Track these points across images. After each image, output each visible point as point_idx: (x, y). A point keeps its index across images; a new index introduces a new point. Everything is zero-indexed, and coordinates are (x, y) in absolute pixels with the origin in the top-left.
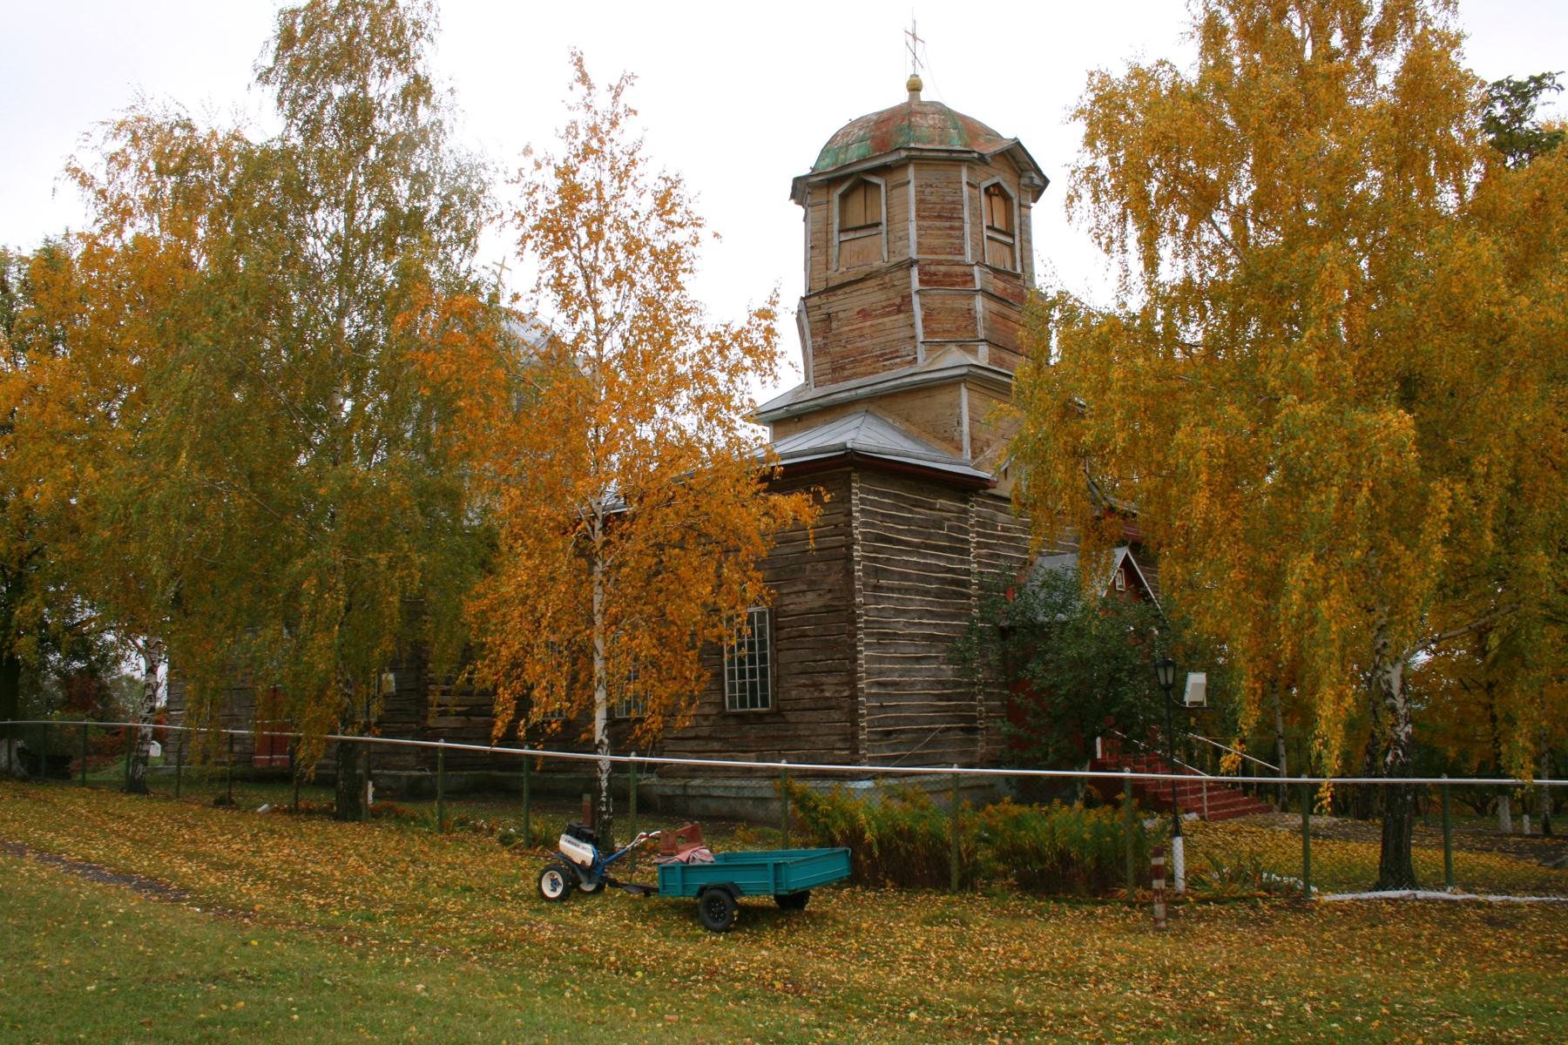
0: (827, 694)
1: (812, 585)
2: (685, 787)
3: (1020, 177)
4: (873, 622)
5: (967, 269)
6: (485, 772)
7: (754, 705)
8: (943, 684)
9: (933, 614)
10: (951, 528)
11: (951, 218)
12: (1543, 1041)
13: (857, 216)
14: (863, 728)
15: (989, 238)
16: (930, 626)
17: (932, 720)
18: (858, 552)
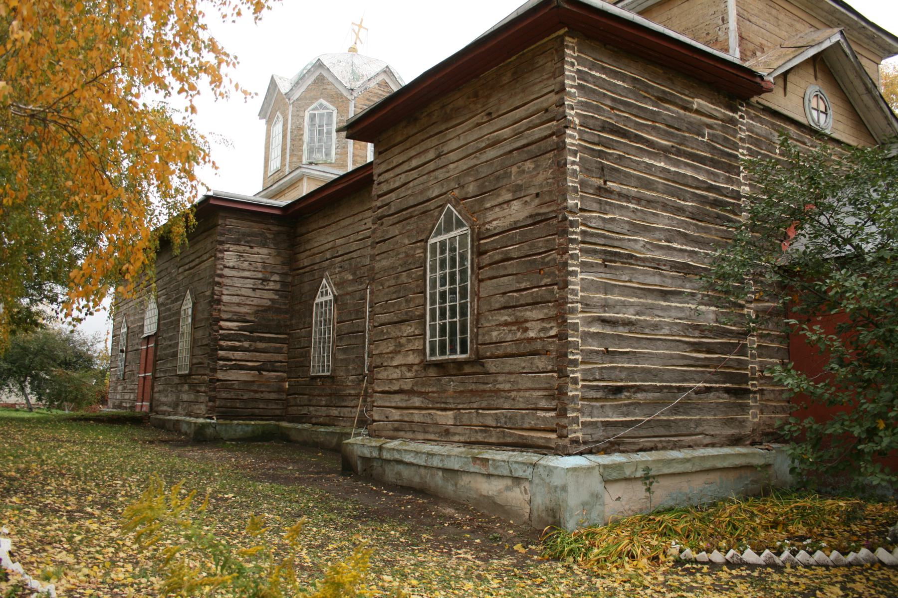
0: (531, 334)
1: (518, 191)
4: (592, 235)
6: (273, 422)
7: (453, 351)
10: (712, 137)
14: (575, 381)
18: (572, 139)
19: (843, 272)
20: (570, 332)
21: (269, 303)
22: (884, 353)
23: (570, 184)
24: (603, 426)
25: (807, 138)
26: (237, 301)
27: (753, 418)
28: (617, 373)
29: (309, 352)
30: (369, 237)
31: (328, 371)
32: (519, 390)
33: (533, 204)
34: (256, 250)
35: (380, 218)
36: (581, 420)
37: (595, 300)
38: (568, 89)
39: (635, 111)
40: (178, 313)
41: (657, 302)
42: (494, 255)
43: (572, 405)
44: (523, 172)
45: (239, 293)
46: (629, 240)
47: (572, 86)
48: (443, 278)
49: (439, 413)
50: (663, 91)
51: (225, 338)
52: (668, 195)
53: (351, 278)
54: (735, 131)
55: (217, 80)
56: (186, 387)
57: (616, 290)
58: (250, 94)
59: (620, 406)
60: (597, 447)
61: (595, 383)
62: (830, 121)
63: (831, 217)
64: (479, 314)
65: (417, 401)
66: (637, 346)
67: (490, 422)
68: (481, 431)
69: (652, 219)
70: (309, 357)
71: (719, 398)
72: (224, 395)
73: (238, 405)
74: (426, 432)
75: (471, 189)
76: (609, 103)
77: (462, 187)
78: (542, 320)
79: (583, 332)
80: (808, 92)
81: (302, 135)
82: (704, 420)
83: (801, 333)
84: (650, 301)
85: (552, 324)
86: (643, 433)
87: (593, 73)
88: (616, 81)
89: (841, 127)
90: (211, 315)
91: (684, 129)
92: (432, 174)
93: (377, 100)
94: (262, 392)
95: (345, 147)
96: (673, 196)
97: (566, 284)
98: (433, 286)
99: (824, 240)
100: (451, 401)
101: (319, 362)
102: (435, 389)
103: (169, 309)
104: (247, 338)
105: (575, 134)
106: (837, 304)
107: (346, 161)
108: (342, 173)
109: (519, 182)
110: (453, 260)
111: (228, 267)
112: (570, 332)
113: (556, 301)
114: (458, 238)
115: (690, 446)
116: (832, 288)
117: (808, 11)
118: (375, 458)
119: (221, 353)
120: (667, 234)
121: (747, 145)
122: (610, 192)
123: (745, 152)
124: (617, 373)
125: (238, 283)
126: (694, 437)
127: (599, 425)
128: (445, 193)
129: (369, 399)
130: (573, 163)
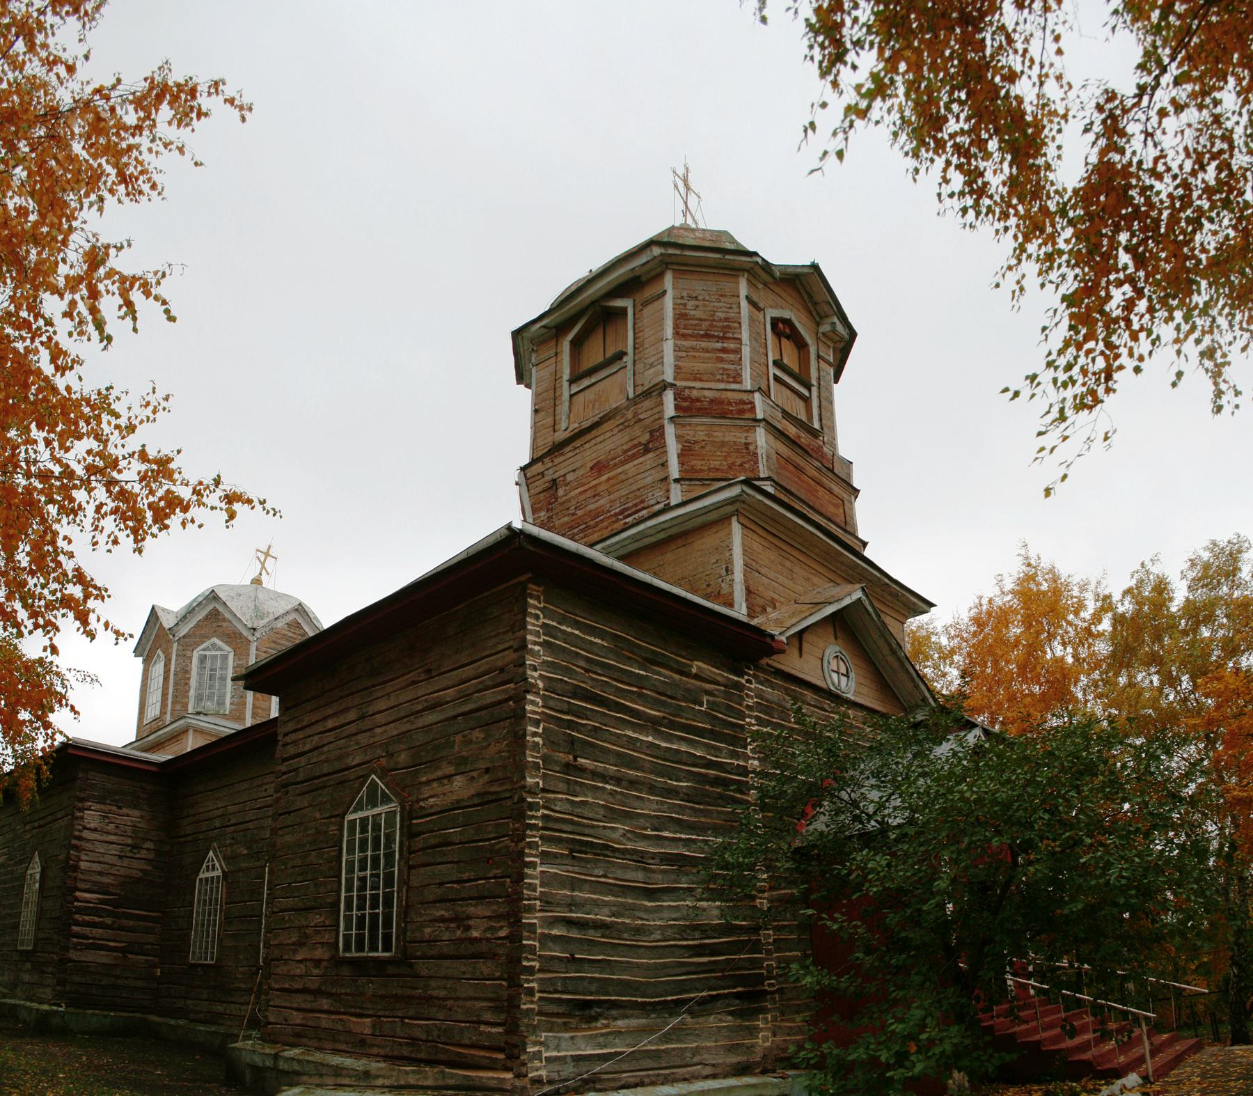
0: (475, 934)
1: (462, 766)
2: (276, 1057)
3: (818, 324)
4: (557, 820)
5: (745, 397)
8: (705, 930)
9: (682, 825)
11: (724, 339)
13: (594, 353)
14: (530, 992)
15: (776, 378)
16: (675, 842)
17: (682, 987)
18: (534, 705)
19: (864, 853)
20: (525, 934)
21: (140, 874)
22: (911, 935)
23: (530, 759)
24: (573, 1061)
25: (827, 704)
26: (99, 869)
27: (764, 1042)
28: (586, 984)
29: (189, 935)
30: (270, 806)
31: (212, 959)
32: (457, 999)
33: (481, 781)
34: (125, 811)
35: (285, 786)
36: (545, 1055)
37: (558, 897)
38: (530, 646)
39: (616, 675)
40: (23, 877)
41: (638, 902)
42: (429, 838)
43: (533, 1038)
44: (471, 742)
45: (101, 859)
46: (605, 827)
47: (535, 643)
48: (363, 862)
49: (354, 1019)
50: (654, 651)
51: (81, 911)
52: (658, 775)
53: (245, 852)
54: (741, 697)
55: (83, 617)
56: (28, 966)
57: (587, 886)
58: (123, 635)
59: (596, 1036)
60: (566, 1086)
61: (556, 996)
62: (853, 684)
63: (852, 791)
64: (408, 906)
65: (325, 1003)
66: (612, 953)
67: (418, 1033)
68: (407, 1044)
69: (636, 804)
70: (189, 940)
71: (721, 1021)
72: (77, 979)
73: (94, 992)
74: (335, 1041)
75: (403, 758)
76: (582, 664)
77: (390, 755)
78: (490, 918)
79: (542, 934)
80: (827, 653)
81: (189, 679)
82: (703, 1048)
83: (820, 923)
84: (630, 901)
85: (502, 924)
86: (625, 1067)
87: (564, 628)
88: (592, 639)
89: (865, 690)
90: (65, 883)
91: (680, 696)
92: (353, 738)
93: (286, 645)
94: (126, 978)
95: (243, 697)
96: (662, 777)
97: (522, 876)
98: (350, 870)
99: (845, 818)
100: (369, 1006)
101: (201, 947)
102: (348, 991)
103: (12, 872)
104: (109, 914)
105: (538, 700)
106: (858, 887)
107: (244, 714)
108: (240, 728)
109: (464, 754)
110: (376, 841)
111: (89, 829)
112: (525, 934)
113: (509, 896)
114: (383, 815)
115: (685, 1079)
116: (853, 871)
117: (826, 563)
118: (269, 1068)
119: (76, 928)
120: (655, 821)
121: (756, 714)
122: (582, 770)
123: (753, 721)
124: (586, 984)
125: (101, 848)
126: (690, 1069)
127: (569, 1060)
128: (368, 762)
129: (263, 997)
130: (535, 734)
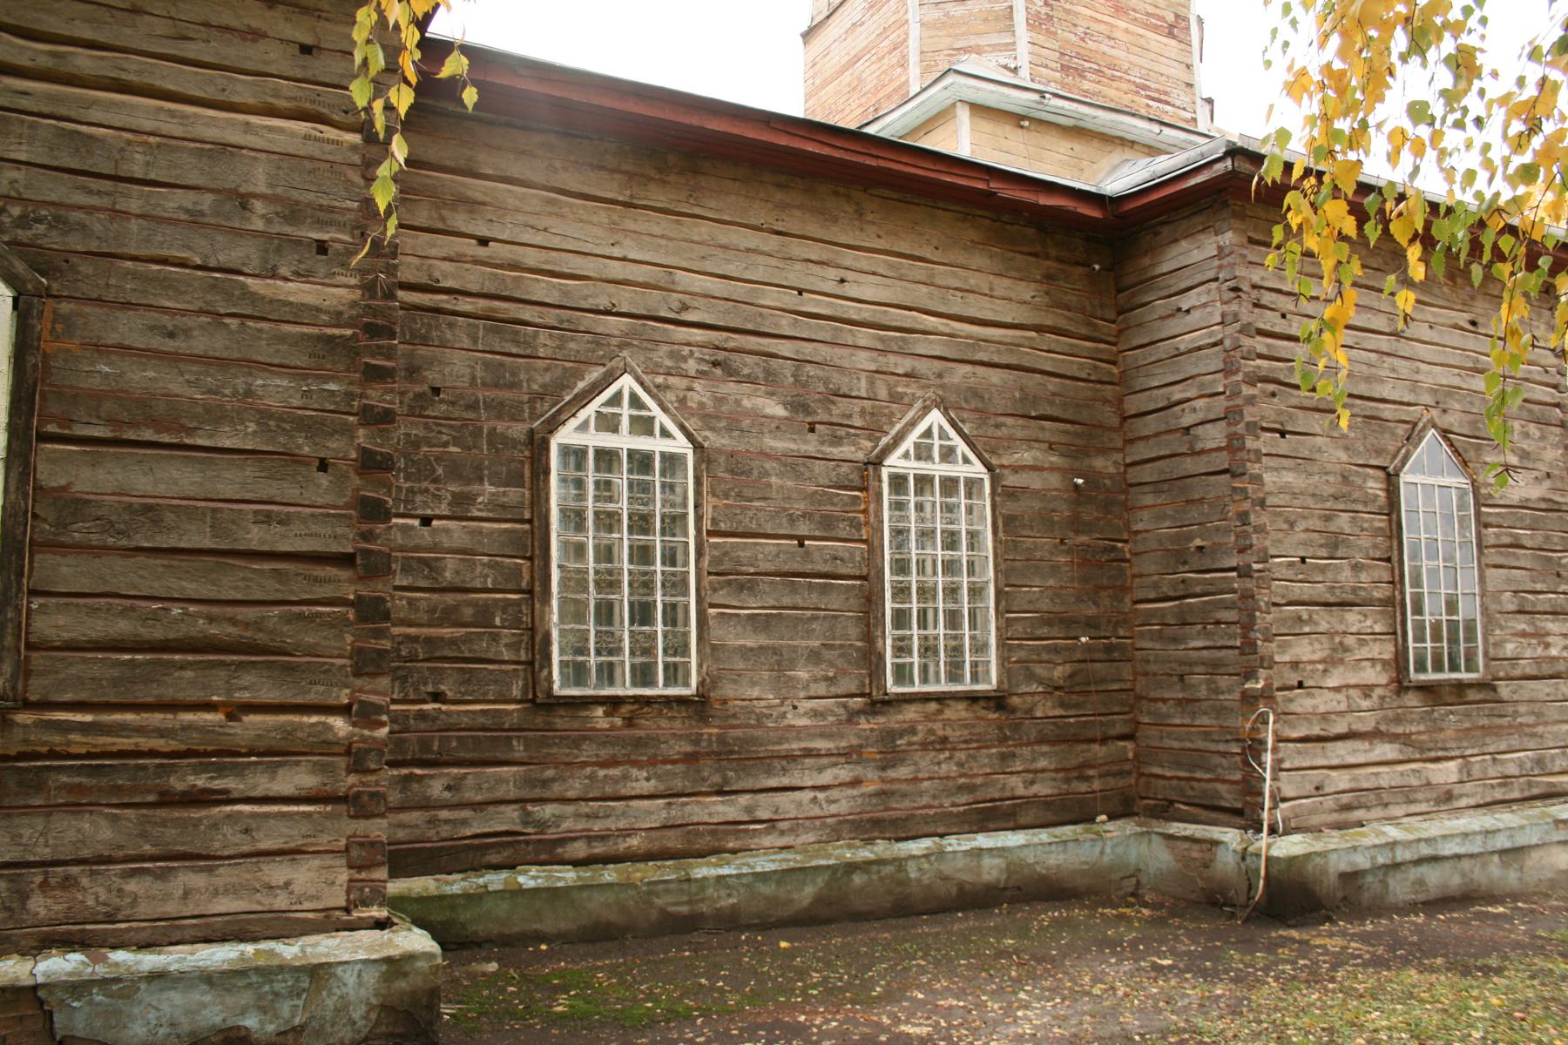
0: (1554, 652)
12: (1461, 1040)
